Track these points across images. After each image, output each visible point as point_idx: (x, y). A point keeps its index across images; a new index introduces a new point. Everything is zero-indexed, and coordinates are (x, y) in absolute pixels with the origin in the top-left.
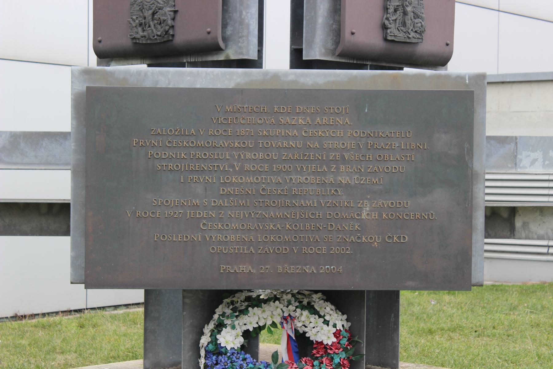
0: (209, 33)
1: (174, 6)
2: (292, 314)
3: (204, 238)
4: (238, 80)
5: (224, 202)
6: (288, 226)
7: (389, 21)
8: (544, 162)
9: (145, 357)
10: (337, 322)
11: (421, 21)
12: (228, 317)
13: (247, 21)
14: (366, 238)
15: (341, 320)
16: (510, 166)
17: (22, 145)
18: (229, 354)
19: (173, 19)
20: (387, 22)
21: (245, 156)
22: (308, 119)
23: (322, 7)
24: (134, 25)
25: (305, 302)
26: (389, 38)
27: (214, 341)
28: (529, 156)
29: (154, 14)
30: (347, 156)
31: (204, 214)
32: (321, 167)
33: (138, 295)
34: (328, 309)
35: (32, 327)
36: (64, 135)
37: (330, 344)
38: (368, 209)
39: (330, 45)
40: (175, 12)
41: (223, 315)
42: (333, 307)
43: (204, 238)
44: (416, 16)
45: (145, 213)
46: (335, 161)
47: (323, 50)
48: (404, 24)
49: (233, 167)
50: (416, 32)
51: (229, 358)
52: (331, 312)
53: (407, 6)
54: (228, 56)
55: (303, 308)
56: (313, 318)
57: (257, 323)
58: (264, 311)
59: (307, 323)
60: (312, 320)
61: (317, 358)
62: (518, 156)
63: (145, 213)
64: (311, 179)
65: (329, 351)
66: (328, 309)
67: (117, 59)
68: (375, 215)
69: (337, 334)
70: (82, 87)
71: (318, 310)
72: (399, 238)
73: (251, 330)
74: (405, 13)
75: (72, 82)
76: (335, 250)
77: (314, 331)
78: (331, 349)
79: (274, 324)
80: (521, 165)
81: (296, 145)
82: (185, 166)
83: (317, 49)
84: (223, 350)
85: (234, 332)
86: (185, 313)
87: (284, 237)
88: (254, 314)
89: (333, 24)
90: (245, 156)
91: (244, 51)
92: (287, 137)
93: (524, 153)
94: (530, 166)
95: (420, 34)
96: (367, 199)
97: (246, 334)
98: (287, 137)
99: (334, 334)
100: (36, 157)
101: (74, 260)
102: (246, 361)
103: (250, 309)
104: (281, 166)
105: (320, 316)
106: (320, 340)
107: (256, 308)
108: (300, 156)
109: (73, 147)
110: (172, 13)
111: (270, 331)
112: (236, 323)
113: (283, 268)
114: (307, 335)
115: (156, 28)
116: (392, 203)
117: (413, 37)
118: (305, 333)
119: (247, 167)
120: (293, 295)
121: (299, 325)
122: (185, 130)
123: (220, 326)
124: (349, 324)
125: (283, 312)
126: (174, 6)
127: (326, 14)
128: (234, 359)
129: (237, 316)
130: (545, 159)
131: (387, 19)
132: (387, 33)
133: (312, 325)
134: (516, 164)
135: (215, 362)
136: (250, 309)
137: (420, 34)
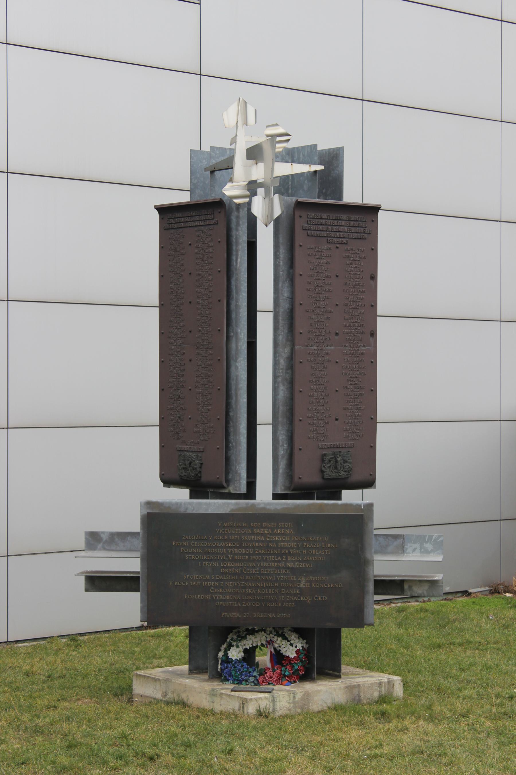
0: (218, 478)
1: (201, 460)
2: (272, 639)
3: (212, 597)
4: (232, 507)
5: (223, 577)
6: (259, 591)
7: (325, 467)
8: (421, 550)
9: (190, 664)
10: (297, 645)
11: (349, 464)
12: (235, 641)
13: (239, 472)
14: (303, 598)
15: (302, 643)
16: (400, 552)
17: (116, 539)
18: (233, 663)
19: (201, 467)
20: (323, 469)
21: (235, 551)
22: (270, 530)
23: (281, 463)
24: (180, 468)
25: (280, 632)
26: (326, 477)
27: (226, 654)
28: (411, 546)
29: (190, 463)
30: (291, 551)
31: (212, 584)
32: (277, 558)
33: (188, 627)
34: (293, 637)
35: (150, 637)
36: (137, 533)
37: (293, 657)
38: (304, 581)
39: (287, 485)
40: (202, 464)
41: (232, 639)
42: (297, 636)
43: (212, 597)
44: (345, 462)
45: (180, 583)
46: (285, 554)
47: (283, 488)
48: (336, 468)
49: (228, 557)
50: (345, 471)
51: (233, 665)
52: (295, 639)
53: (338, 457)
54: (229, 490)
55: (279, 635)
56: (284, 642)
57: (252, 644)
58: (256, 637)
59: (281, 645)
60: (283, 643)
61: (284, 666)
62: (405, 546)
63: (180, 583)
64: (272, 564)
65: (292, 662)
66: (293, 637)
67: (172, 486)
68: (308, 585)
69: (298, 652)
70: (145, 512)
71: (287, 637)
72: (322, 598)
73: (248, 648)
74: (336, 461)
75: (140, 509)
76: (285, 605)
77: (285, 649)
78: (293, 661)
79: (262, 645)
80: (407, 552)
81: (263, 545)
82: (201, 557)
83: (279, 488)
84: (230, 660)
85: (238, 650)
86: (210, 638)
87: (257, 597)
88: (250, 639)
89: (289, 472)
90: (235, 551)
91: (238, 489)
92: (258, 541)
93: (409, 545)
94: (412, 552)
95: (349, 472)
96: (303, 576)
97: (246, 651)
98: (258, 541)
99: (296, 651)
100: (124, 546)
101: (142, 608)
102: (153, 666)
103: (248, 636)
104: (254, 557)
105: (288, 641)
106: (287, 655)
107: (251, 636)
108: (265, 551)
109: (141, 545)
110: (200, 464)
111: (261, 649)
112: (239, 644)
113: (257, 615)
114: (281, 652)
115: (192, 472)
116: (318, 578)
117: (343, 475)
118: (280, 650)
119: (236, 557)
120: (274, 628)
121: (276, 646)
122: (201, 537)
123: (230, 646)
124: (308, 645)
125: (267, 638)
126: (201, 460)
127: (284, 467)
128: (236, 665)
129: (240, 640)
130: (421, 548)
131: (324, 467)
132: (324, 475)
133: (283, 646)
134: (404, 551)
135: (226, 667)
136: (248, 636)
137: (349, 472)
